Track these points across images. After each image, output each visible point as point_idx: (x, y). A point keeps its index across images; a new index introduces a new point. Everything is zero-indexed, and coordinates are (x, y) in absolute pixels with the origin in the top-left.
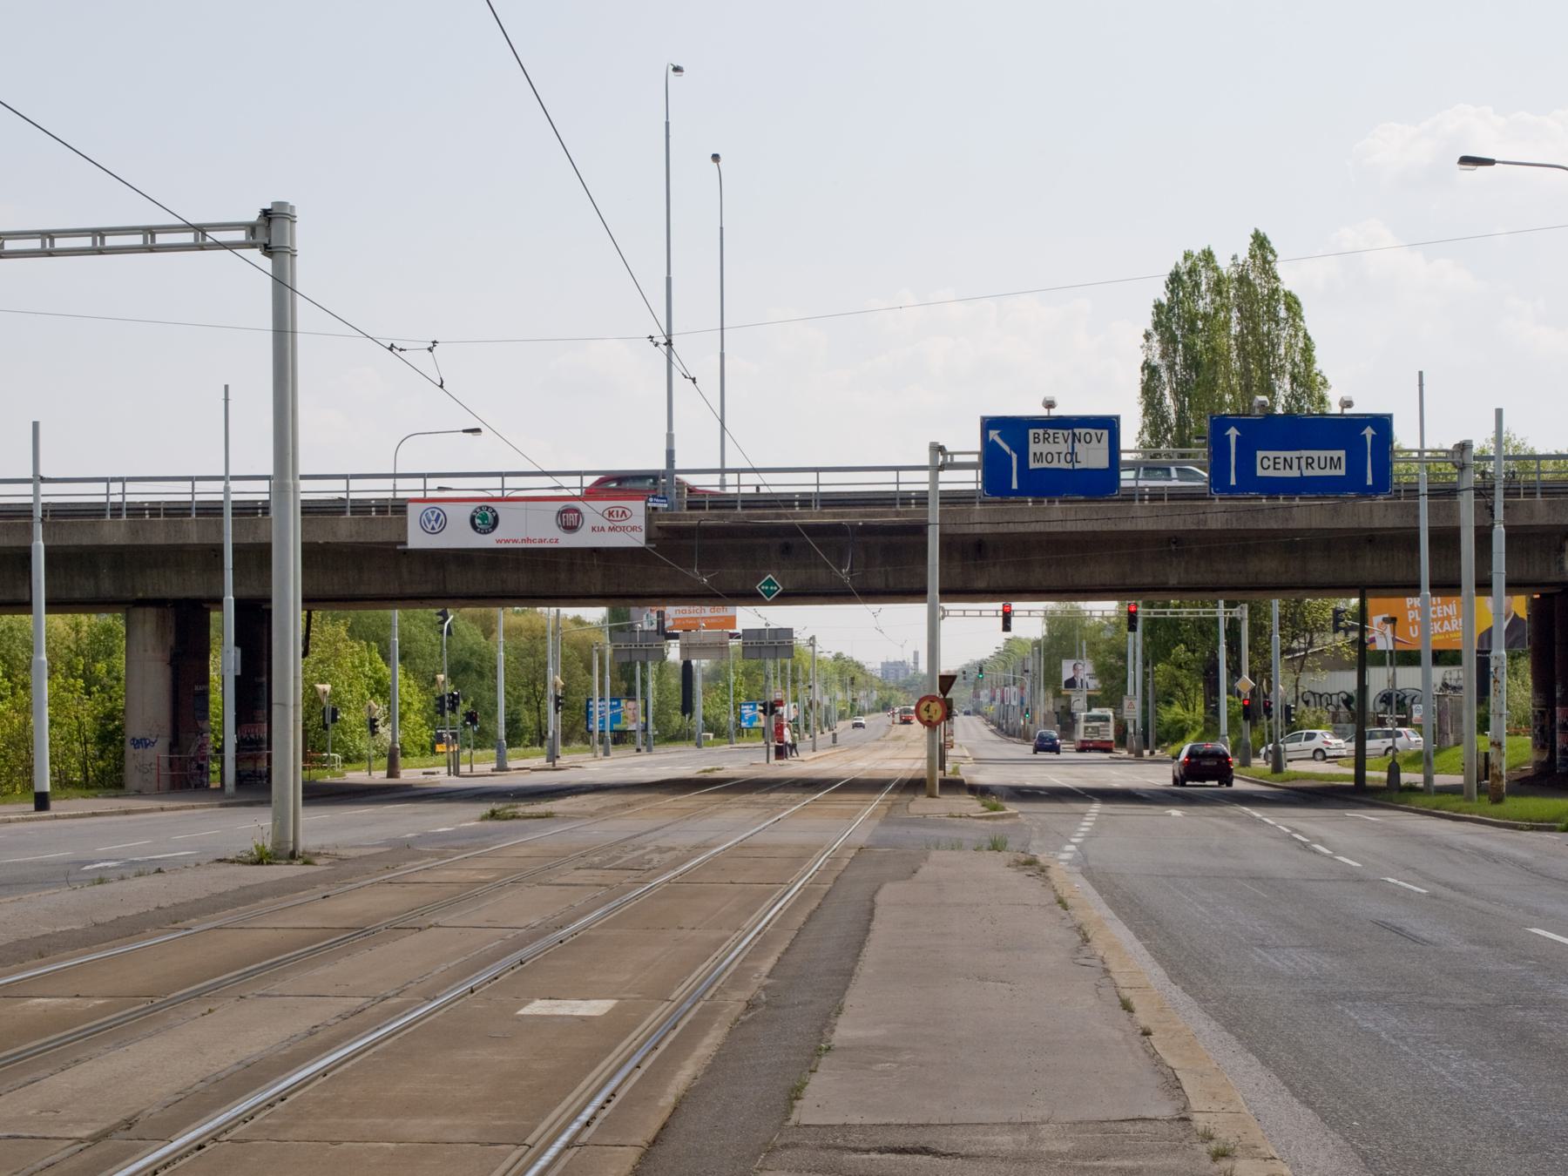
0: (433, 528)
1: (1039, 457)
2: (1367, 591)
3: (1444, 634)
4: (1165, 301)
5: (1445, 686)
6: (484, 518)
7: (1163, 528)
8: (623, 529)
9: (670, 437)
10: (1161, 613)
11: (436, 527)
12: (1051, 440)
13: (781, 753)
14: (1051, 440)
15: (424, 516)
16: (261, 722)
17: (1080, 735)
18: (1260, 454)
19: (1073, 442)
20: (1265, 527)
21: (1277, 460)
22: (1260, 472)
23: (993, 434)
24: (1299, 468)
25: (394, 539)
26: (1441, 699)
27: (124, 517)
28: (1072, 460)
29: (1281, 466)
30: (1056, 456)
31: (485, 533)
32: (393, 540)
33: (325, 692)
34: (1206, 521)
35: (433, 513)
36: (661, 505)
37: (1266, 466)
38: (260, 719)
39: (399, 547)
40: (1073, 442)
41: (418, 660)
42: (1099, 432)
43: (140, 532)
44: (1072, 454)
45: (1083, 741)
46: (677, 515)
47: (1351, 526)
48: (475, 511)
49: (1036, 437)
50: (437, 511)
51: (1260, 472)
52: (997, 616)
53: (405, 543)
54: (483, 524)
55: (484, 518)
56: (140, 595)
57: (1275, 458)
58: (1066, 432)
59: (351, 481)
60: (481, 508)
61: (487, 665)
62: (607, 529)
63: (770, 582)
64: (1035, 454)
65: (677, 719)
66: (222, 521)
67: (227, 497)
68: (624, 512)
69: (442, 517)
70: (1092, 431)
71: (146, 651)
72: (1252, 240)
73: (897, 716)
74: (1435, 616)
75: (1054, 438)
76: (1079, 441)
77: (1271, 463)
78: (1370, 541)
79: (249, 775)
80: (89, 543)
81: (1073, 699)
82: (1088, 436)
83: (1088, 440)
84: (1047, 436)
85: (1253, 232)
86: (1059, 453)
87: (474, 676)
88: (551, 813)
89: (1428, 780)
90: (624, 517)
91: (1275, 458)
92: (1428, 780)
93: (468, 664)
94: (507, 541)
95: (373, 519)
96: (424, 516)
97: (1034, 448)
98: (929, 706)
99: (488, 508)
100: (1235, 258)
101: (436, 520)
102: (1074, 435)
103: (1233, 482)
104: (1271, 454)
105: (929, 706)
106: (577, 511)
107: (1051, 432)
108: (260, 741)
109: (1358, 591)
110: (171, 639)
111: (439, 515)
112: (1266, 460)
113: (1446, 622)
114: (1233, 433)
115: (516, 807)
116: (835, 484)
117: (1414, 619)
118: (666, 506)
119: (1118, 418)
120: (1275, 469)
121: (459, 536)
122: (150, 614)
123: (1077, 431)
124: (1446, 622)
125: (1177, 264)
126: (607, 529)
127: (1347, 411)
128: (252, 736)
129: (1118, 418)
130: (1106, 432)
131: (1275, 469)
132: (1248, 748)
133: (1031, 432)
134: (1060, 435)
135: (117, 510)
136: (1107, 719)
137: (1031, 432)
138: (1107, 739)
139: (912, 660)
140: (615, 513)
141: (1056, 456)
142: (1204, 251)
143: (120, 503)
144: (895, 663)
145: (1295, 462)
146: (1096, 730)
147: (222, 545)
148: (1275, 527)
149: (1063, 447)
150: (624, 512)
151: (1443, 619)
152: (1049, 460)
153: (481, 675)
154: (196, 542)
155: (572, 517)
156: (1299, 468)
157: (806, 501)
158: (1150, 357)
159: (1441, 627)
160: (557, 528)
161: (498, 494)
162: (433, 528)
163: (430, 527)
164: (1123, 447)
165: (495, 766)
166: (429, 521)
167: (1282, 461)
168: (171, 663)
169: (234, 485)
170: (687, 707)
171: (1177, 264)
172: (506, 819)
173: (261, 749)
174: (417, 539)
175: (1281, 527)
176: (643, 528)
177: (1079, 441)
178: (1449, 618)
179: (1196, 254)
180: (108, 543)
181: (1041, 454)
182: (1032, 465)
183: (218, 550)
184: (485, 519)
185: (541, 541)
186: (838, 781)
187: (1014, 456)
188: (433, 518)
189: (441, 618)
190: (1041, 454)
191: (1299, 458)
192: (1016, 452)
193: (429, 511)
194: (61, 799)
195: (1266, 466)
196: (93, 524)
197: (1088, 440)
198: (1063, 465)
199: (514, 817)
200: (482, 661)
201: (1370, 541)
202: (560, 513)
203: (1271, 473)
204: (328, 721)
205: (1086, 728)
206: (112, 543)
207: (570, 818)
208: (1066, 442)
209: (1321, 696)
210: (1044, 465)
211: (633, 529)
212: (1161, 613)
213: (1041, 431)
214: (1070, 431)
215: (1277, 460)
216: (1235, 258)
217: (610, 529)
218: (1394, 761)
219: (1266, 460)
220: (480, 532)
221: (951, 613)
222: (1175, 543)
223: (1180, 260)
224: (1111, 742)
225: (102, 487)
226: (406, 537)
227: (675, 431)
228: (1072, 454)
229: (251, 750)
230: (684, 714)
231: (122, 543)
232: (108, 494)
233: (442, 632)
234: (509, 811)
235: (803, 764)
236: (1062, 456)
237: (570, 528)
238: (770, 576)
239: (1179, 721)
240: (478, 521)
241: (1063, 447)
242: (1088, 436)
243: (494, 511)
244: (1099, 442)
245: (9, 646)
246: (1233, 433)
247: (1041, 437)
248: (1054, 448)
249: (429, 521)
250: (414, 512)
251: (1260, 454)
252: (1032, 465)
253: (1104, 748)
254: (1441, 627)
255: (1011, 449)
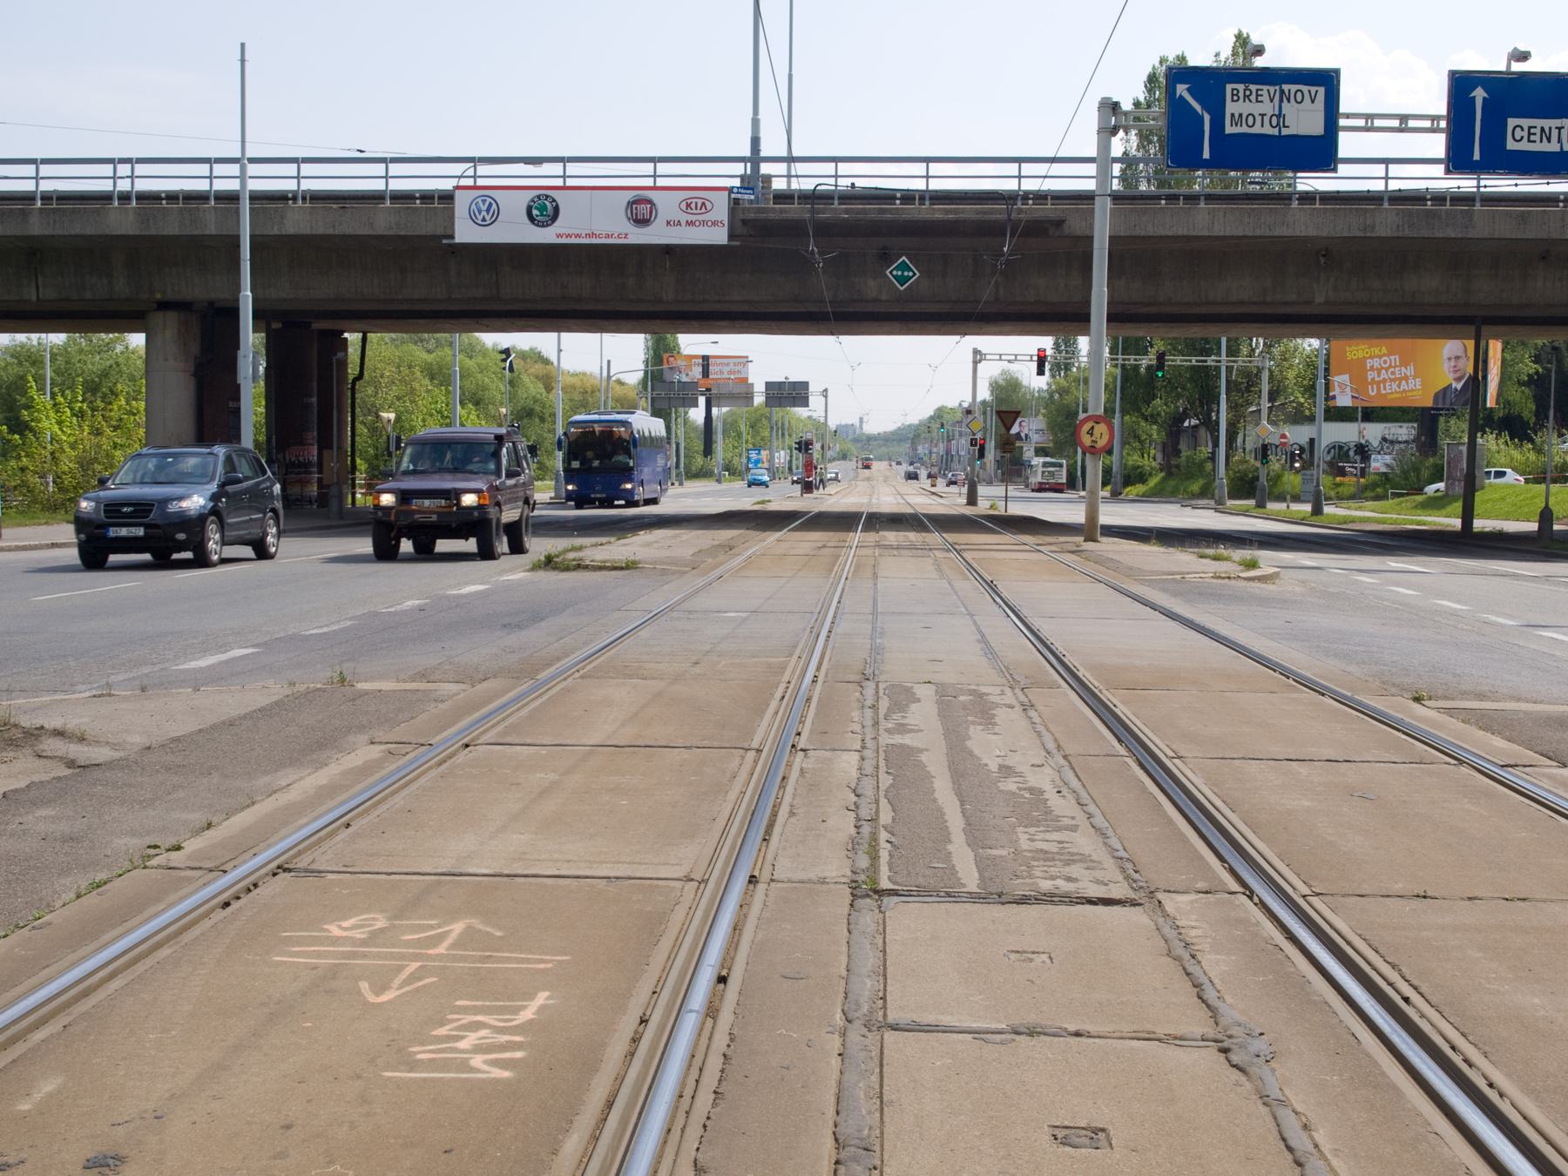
0: (484, 220)
1: (1238, 119)
2: (1485, 329)
3: (1401, 392)
4: (1142, 99)
5: (1384, 439)
6: (542, 208)
7: (1324, 234)
8: (704, 223)
9: (756, 123)
10: (1186, 361)
11: (488, 218)
12: (1253, 98)
13: (808, 487)
14: (1253, 98)
15: (474, 206)
16: (310, 444)
17: (1036, 479)
18: (1512, 122)
19: (1281, 101)
20: (1441, 236)
21: (1532, 131)
22: (1511, 145)
23: (1182, 89)
24: (1559, 141)
25: (440, 231)
26: (1451, 447)
27: (134, 203)
28: (1278, 124)
29: (1537, 138)
30: (1259, 119)
31: (543, 226)
32: (438, 233)
33: (389, 421)
34: (1373, 227)
35: (484, 201)
36: (746, 197)
37: (1518, 138)
38: (309, 442)
39: (444, 241)
40: (1281, 101)
41: (490, 407)
42: (1313, 89)
43: (151, 221)
44: (1278, 116)
45: (1040, 483)
46: (763, 208)
47: (1539, 237)
48: (533, 201)
49: (1235, 93)
50: (489, 200)
51: (1511, 145)
52: (1031, 360)
53: (452, 237)
54: (542, 215)
55: (542, 208)
56: (158, 296)
57: (1530, 128)
58: (1272, 89)
59: (390, 165)
60: (539, 197)
61: (547, 412)
62: (683, 223)
63: (904, 267)
64: (1233, 115)
65: (699, 460)
66: (238, 208)
67: (243, 184)
68: (703, 204)
69: (494, 206)
70: (1305, 88)
71: (166, 360)
72: (1235, 39)
73: (860, 462)
74: (1393, 377)
75: (1257, 95)
76: (1289, 101)
77: (1525, 134)
78: (1544, 258)
79: (297, 500)
80: (93, 233)
81: (1025, 449)
82: (1299, 94)
83: (1299, 99)
84: (1248, 93)
85: (1236, 32)
86: (1263, 115)
87: (537, 420)
88: (634, 563)
89: (1092, 515)
90: (703, 210)
91: (1530, 128)
92: (1092, 515)
93: (532, 410)
94: (569, 236)
95: (416, 209)
96: (474, 206)
97: (1231, 108)
98: (1092, 428)
99: (547, 196)
100: (1217, 55)
101: (488, 211)
102: (1282, 92)
103: (1477, 156)
104: (1526, 122)
105: (1092, 428)
106: (650, 202)
107: (1253, 87)
108: (310, 464)
109: (1472, 329)
110: (195, 348)
111: (490, 205)
112: (1518, 129)
113: (1404, 382)
114: (1479, 94)
115: (580, 548)
116: (949, 179)
117: (1373, 379)
118: (752, 197)
119: (1337, 72)
120: (1529, 141)
121: (514, 230)
122: (171, 320)
123: (1286, 87)
124: (1404, 382)
125: (1154, 66)
126: (683, 223)
127: (1517, 67)
128: (301, 459)
129: (1337, 72)
130: (1322, 90)
131: (1529, 141)
132: (1264, 490)
133: (1229, 87)
134: (1265, 93)
135: (125, 197)
136: (1061, 466)
137: (1229, 87)
138: (1060, 481)
139: (858, 424)
140: (693, 206)
141: (1259, 119)
142: (1178, 57)
143: (128, 192)
144: (846, 426)
145: (1555, 133)
146: (1052, 474)
147: (239, 236)
148: (1453, 235)
149: (1268, 108)
150: (703, 204)
151: (1400, 380)
152: (1250, 123)
153: (542, 420)
154: (214, 232)
155: (643, 209)
156: (1559, 141)
157: (908, 197)
158: (1129, 149)
159: (1399, 386)
160: (625, 220)
161: (559, 182)
162: (484, 220)
163: (480, 218)
164: (1342, 109)
165: (553, 495)
166: (480, 212)
167: (1538, 131)
168: (195, 375)
169: (253, 169)
170: (708, 450)
171: (1154, 66)
172: (567, 569)
173: (311, 473)
174: (466, 232)
175: (1460, 235)
176: (726, 222)
177: (1289, 101)
178: (1406, 378)
179: (1171, 59)
180: (114, 233)
181: (1241, 115)
182: (1229, 130)
183: (235, 242)
184: (544, 209)
185: (608, 236)
186: (806, 513)
187: (1207, 118)
188: (484, 208)
189: (504, 356)
190: (1241, 115)
191: (1559, 129)
192: (1209, 113)
193: (479, 200)
194: (40, 524)
195: (1518, 138)
196: (98, 211)
197: (1299, 99)
198: (1268, 130)
199: (580, 566)
200: (543, 408)
201: (1544, 258)
202: (631, 204)
203: (1524, 146)
204: (392, 448)
205: (1043, 472)
206: (119, 233)
207: (664, 572)
208: (1272, 101)
209: (1277, 447)
210: (1244, 129)
211: (715, 223)
212: (1186, 361)
213: (1241, 87)
214: (1277, 88)
215: (1532, 131)
216: (1217, 55)
217: (689, 223)
218: (1547, 506)
219: (1518, 129)
220: (538, 225)
221: (988, 357)
222: (1324, 256)
223: (1157, 65)
224: (1063, 484)
225: (107, 170)
226: (453, 230)
227: (761, 116)
228: (1278, 116)
229: (299, 473)
230: (706, 456)
231: (131, 233)
232: (114, 178)
233: (504, 369)
234: (571, 555)
235: (832, 499)
236: (1266, 119)
237: (642, 222)
238: (904, 258)
239: (1138, 467)
240: (535, 212)
241: (1268, 108)
242: (1299, 94)
243: (554, 200)
244: (1313, 101)
245: (117, 379)
246: (1479, 94)
247: (1241, 95)
248: (1256, 109)
249: (480, 212)
250: (462, 203)
251: (1512, 122)
252: (1229, 130)
253: (1057, 489)
254: (1399, 386)
255: (1203, 108)
